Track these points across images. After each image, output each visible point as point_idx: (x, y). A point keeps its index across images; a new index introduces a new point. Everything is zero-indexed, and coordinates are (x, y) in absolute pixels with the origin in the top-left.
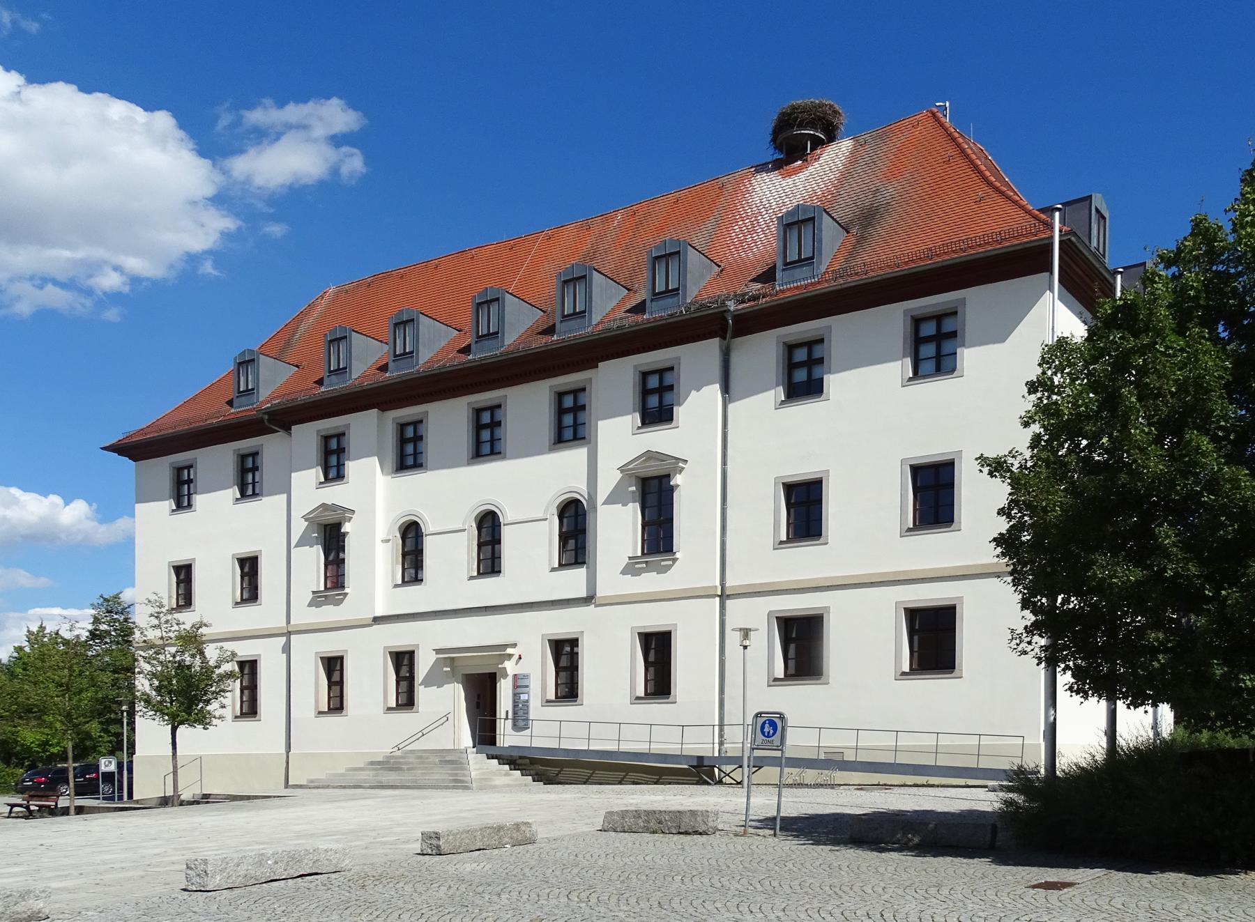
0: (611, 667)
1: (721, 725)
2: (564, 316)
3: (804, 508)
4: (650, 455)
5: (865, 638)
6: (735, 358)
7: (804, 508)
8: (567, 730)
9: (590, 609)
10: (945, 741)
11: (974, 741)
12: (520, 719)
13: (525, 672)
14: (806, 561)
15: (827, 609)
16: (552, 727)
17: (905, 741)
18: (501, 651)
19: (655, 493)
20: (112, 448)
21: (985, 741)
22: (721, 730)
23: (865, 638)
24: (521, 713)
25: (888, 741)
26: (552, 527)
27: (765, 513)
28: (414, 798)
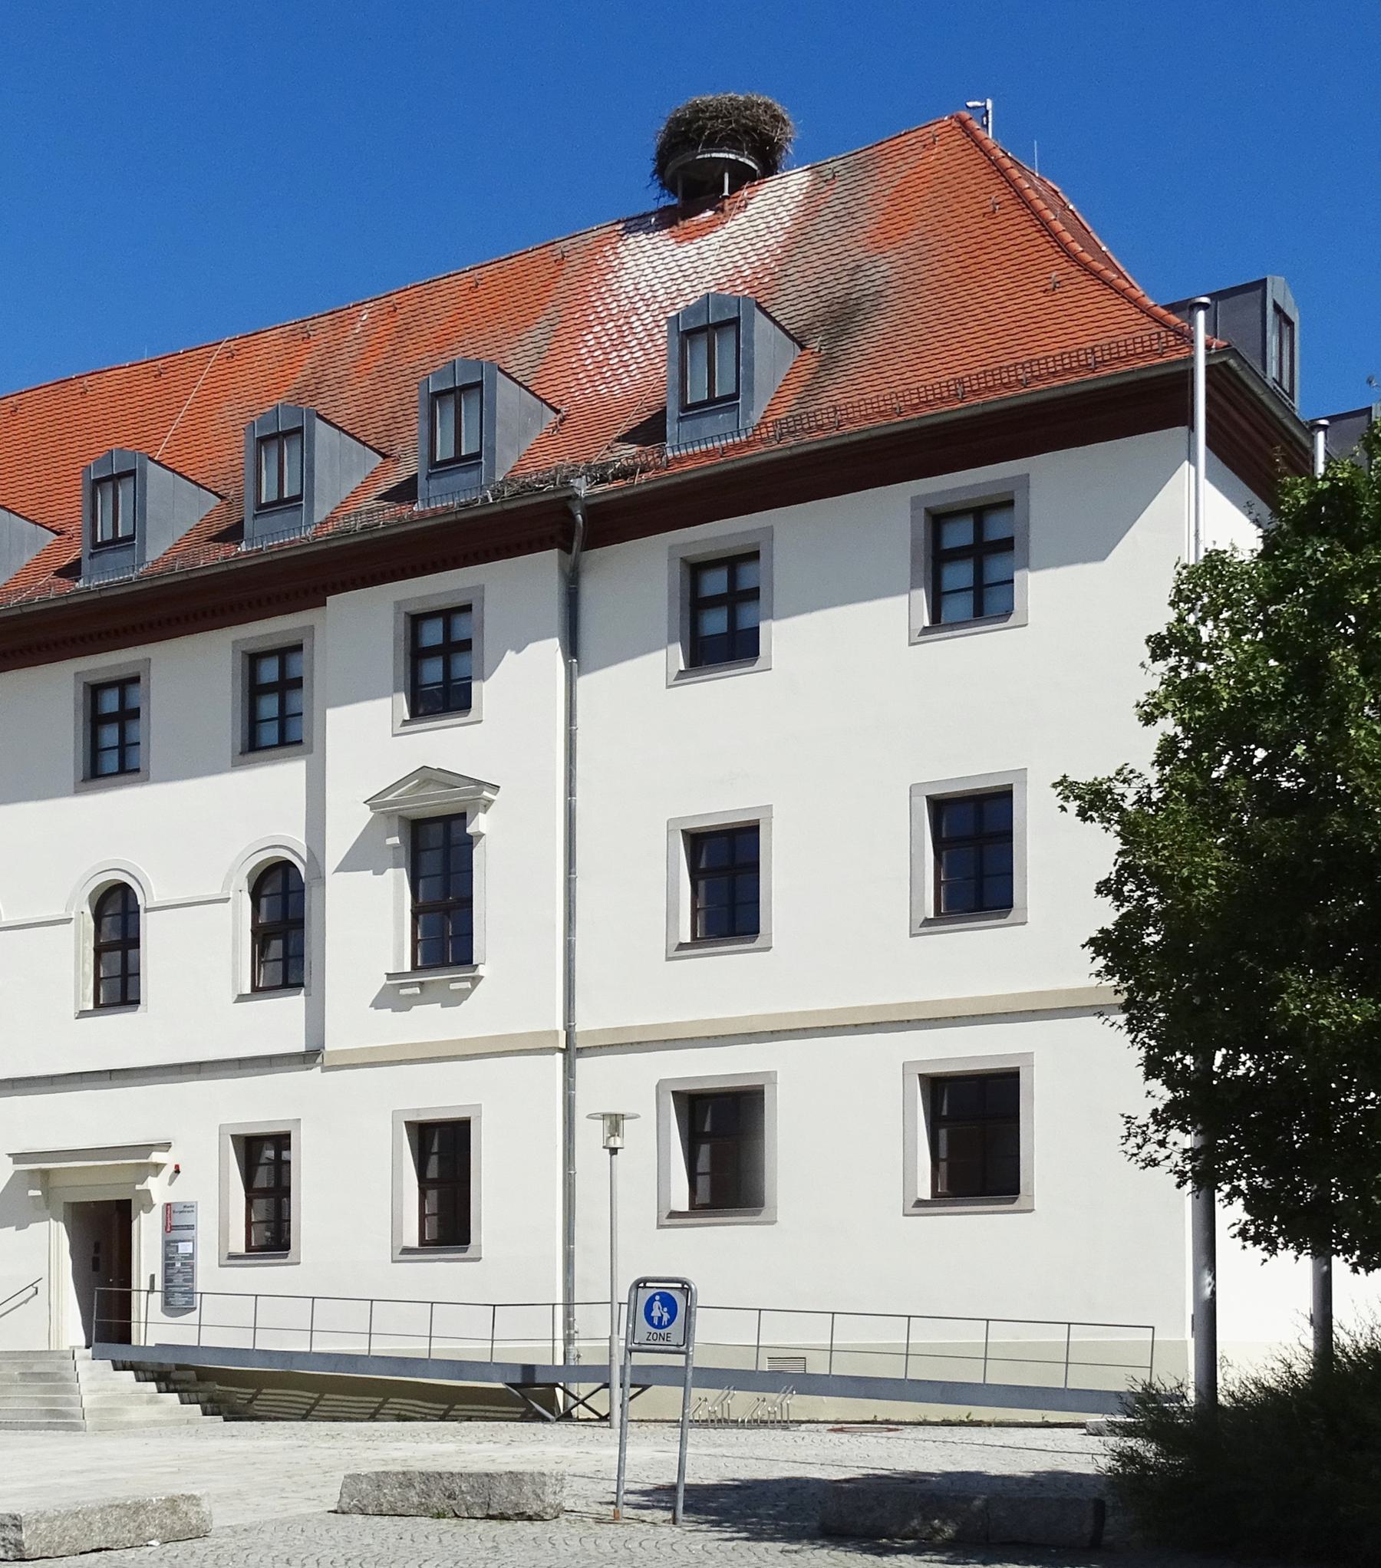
0: (355, 1187)
1: (569, 1304)
3: (725, 881)
7: (725, 881)
10: (1001, 1335)
11: (1058, 1335)
12: (178, 1292)
14: (726, 984)
15: (771, 1076)
16: (237, 1310)
17: (925, 1335)
18: (139, 1157)
19: (437, 852)
21: (1079, 1335)
22: (568, 1314)
23: (846, 1138)
24: (178, 1280)
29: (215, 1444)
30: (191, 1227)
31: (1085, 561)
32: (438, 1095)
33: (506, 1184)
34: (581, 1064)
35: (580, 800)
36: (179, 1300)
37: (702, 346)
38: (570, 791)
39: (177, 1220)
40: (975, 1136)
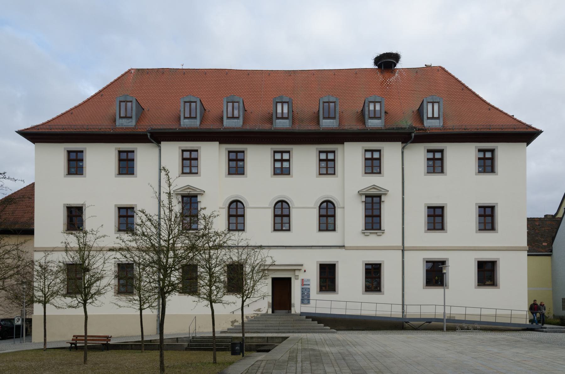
0: (351, 278)
1: (403, 305)
2: (131, 102)
3: (436, 217)
4: (374, 187)
5: (461, 273)
6: (405, 151)
7: (436, 217)
8: (334, 304)
9: (342, 251)
10: (499, 312)
11: (509, 312)
12: (305, 299)
13: (308, 278)
14: (436, 238)
15: (448, 259)
16: (322, 303)
17: (484, 312)
18: (296, 268)
19: (373, 205)
20: (16, 132)
21: (513, 312)
22: (403, 307)
23: (461, 273)
24: (306, 297)
25: (478, 312)
26: (315, 214)
27: (418, 218)
28: (60, 342)
29: (330, 335)
30: (309, 285)
31: (529, 234)
32: (373, 258)
33: (389, 277)
34: (405, 252)
35: (405, 197)
36: (306, 301)
37: (435, 116)
38: (403, 194)
39: (305, 283)
40: (487, 273)
